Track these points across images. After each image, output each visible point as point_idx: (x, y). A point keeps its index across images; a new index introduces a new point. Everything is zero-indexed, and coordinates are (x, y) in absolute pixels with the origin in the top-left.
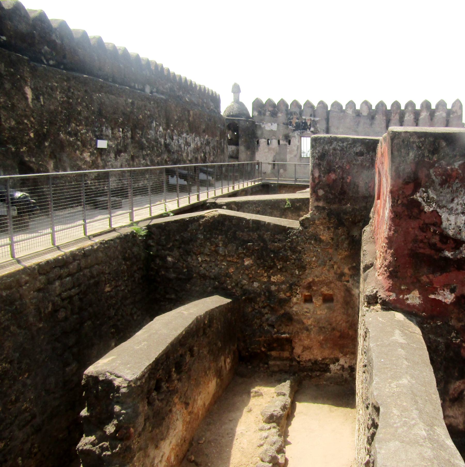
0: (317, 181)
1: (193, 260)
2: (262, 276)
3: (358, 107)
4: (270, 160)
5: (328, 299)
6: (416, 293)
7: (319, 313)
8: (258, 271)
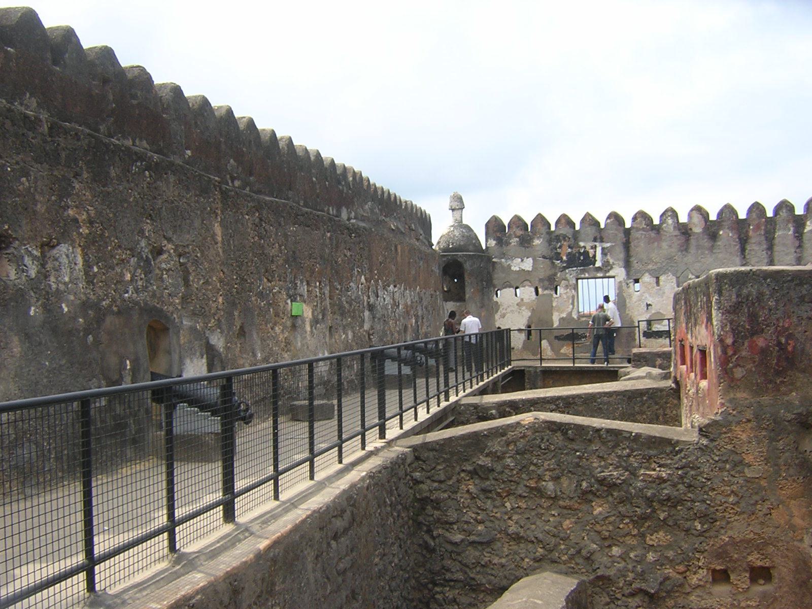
1: (495, 507)
8: (621, 526)
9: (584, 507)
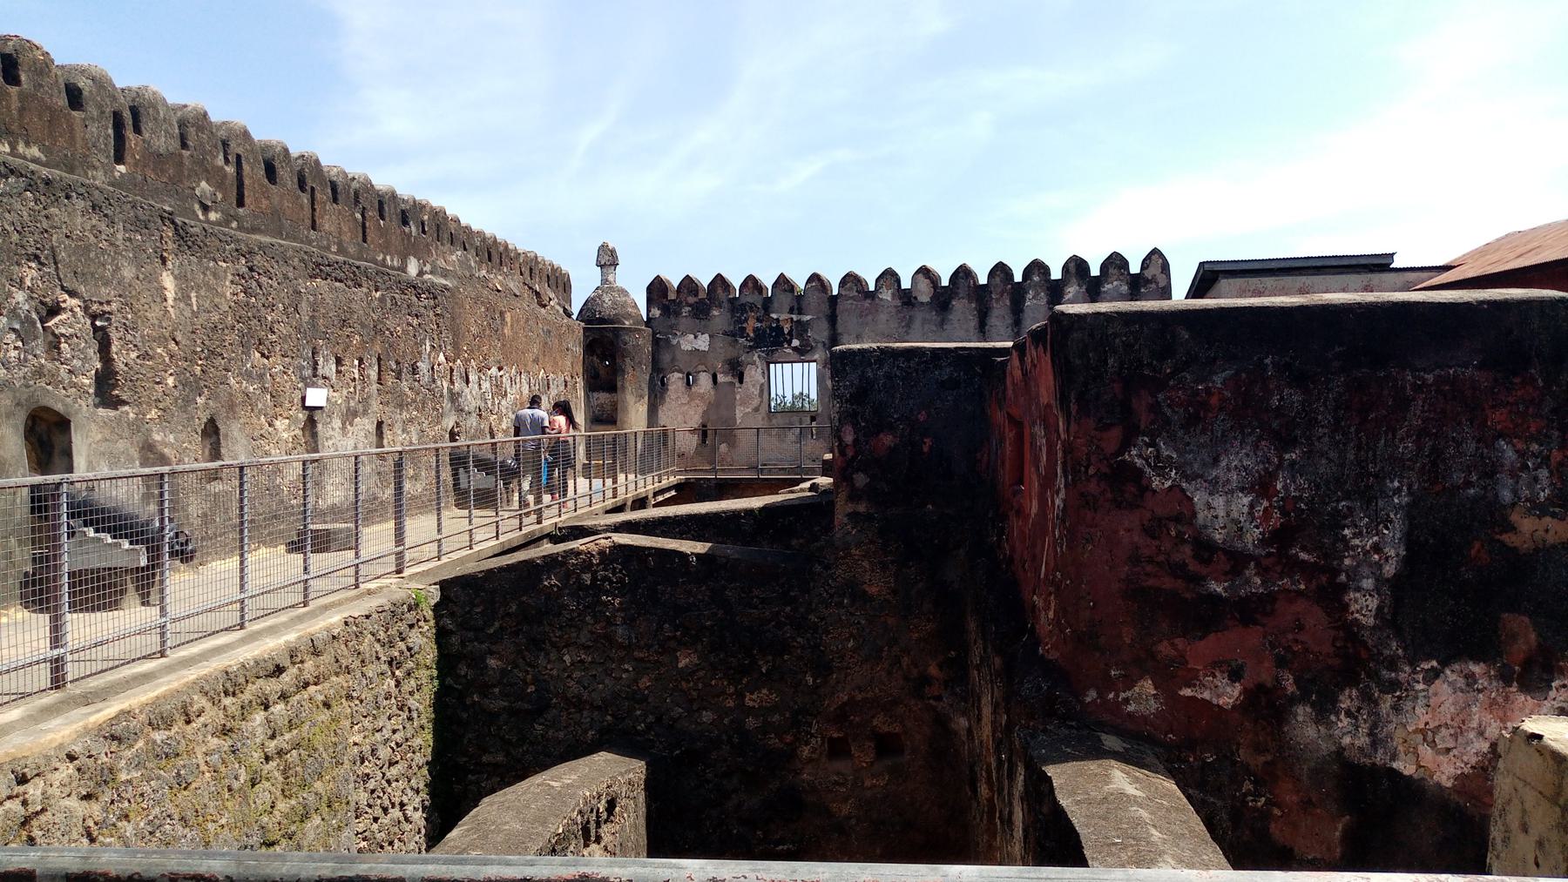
0: (850, 453)
2: (723, 693)
3: (906, 284)
4: (695, 421)
5: (886, 746)
6: (1147, 687)
7: (868, 783)
9: (665, 659)
